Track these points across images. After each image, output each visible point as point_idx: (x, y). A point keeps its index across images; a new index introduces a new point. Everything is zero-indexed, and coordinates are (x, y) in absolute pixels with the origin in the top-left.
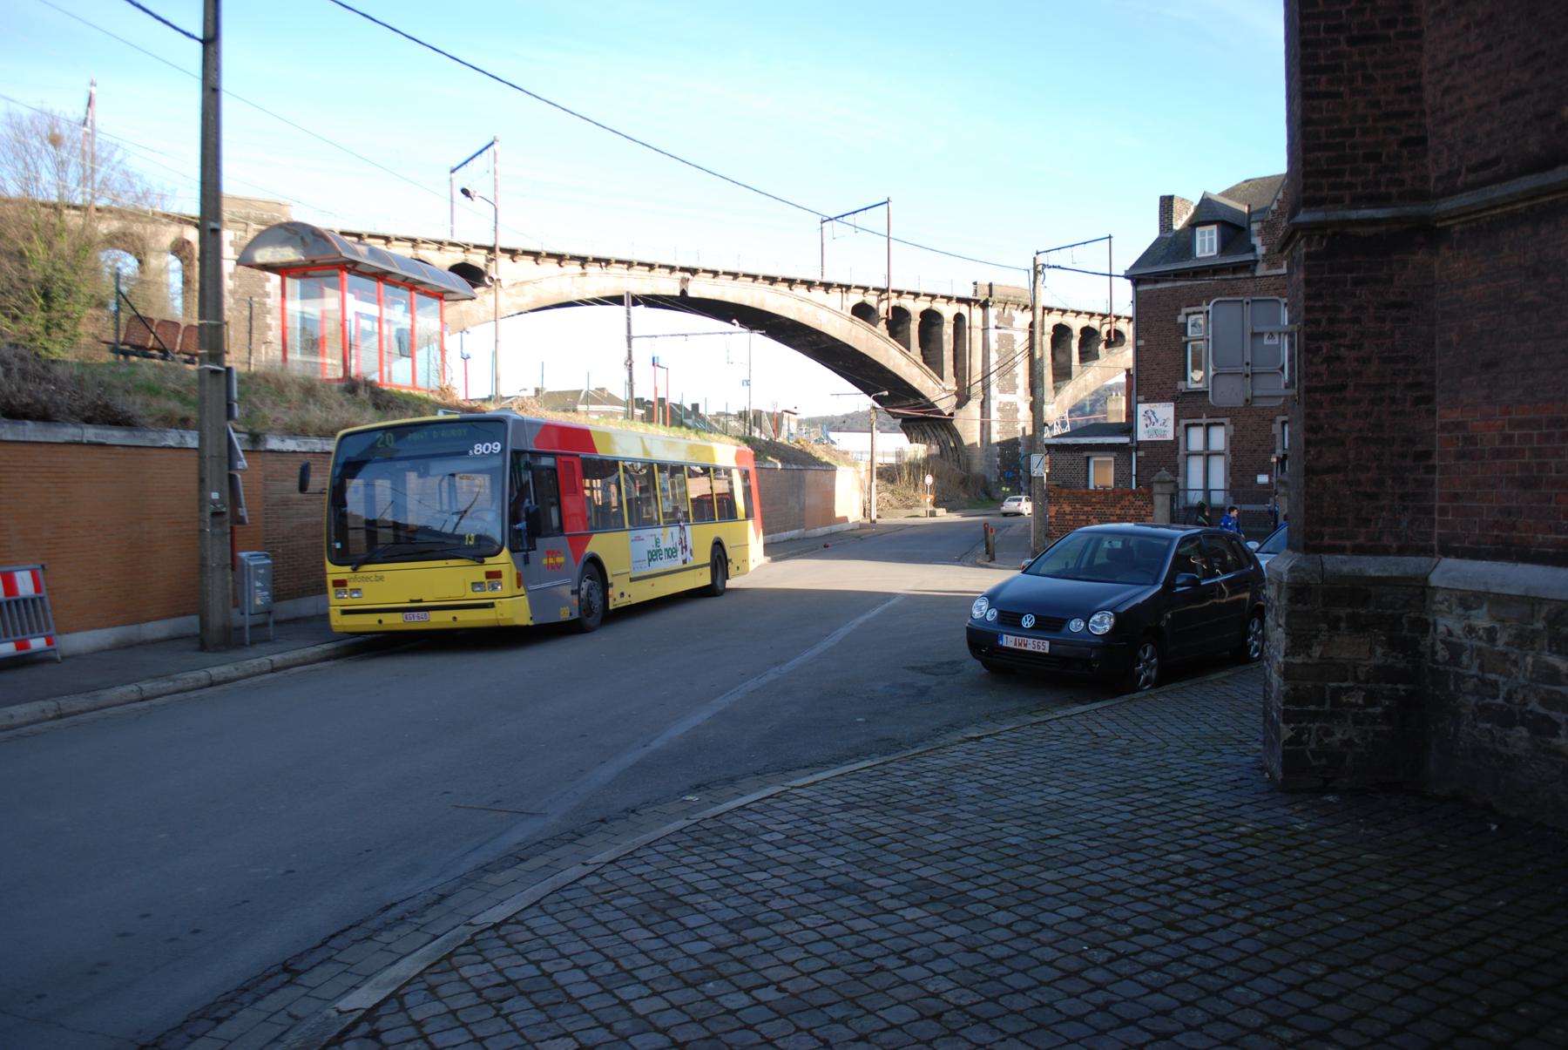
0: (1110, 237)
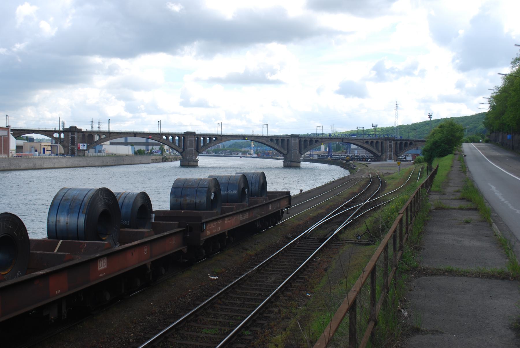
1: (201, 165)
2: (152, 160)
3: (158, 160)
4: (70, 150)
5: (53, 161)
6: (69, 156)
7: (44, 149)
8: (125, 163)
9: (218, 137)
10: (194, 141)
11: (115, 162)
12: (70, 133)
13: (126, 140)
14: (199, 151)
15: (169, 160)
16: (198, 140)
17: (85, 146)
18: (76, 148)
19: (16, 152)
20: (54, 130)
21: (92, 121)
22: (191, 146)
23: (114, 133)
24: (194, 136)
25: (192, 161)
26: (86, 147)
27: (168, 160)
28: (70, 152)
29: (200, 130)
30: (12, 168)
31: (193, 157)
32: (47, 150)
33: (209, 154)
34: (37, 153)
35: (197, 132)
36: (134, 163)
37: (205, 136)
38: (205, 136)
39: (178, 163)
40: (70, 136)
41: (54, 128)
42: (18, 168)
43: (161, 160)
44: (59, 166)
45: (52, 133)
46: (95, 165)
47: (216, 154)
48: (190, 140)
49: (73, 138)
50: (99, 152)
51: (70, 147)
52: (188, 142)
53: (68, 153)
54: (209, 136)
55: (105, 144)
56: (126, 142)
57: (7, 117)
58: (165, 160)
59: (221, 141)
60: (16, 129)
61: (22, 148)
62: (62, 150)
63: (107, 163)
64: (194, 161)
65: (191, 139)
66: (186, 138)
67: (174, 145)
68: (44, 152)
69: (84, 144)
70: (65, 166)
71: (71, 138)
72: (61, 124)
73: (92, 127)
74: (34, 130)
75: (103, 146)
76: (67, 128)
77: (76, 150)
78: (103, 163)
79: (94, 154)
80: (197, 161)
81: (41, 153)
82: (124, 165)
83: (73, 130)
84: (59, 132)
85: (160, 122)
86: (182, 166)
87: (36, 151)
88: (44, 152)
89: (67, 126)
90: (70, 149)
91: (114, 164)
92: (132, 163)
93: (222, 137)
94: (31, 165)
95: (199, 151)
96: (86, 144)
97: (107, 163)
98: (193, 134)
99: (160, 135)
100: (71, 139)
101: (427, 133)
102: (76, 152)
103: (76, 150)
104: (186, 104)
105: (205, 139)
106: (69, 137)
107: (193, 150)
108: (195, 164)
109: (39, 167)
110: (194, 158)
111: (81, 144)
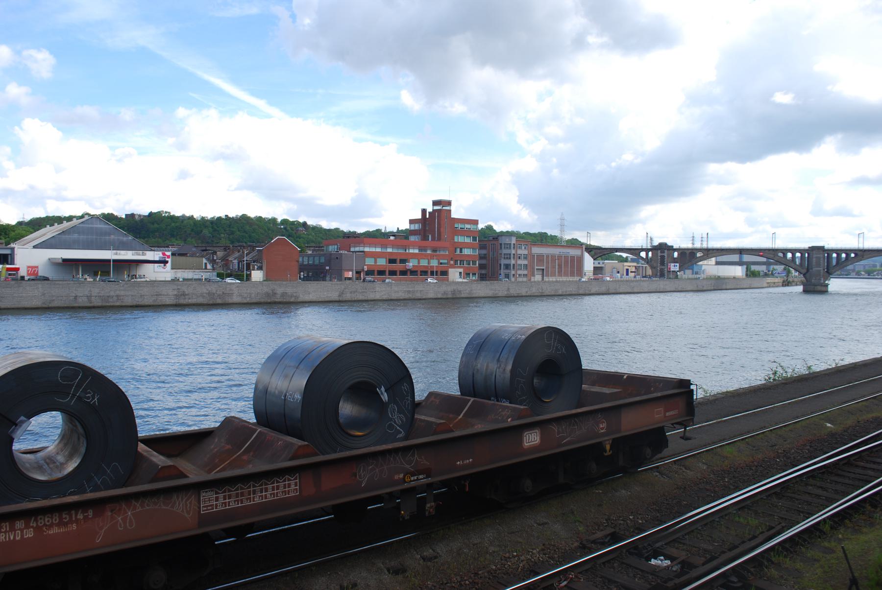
1: (833, 290)
2: (768, 283)
3: (777, 284)
5: (632, 284)
6: (656, 279)
7: (627, 270)
8: (728, 287)
9: (859, 253)
10: (822, 259)
11: (714, 286)
12: (659, 251)
13: (740, 258)
14: (829, 272)
15: (794, 284)
16: (829, 257)
18: (666, 269)
19: (594, 274)
20: (641, 248)
21: (693, 237)
22: (818, 265)
23: (713, 250)
24: (822, 252)
25: (819, 285)
26: (678, 267)
27: (791, 283)
28: (658, 274)
29: (830, 243)
30: (581, 292)
31: (821, 280)
32: (631, 272)
33: (847, 275)
34: (619, 275)
35: (827, 247)
36: (741, 287)
37: (838, 252)
38: (838, 252)
39: (800, 288)
40: (659, 254)
41: (641, 245)
42: (587, 292)
43: (781, 284)
44: (639, 291)
45: (638, 251)
46: (686, 290)
47: (869, 275)
48: (816, 257)
49: (663, 257)
50: (697, 273)
52: (814, 259)
53: (657, 275)
54: (855, 252)
55: (709, 264)
56: (741, 261)
57: (589, 235)
58: (786, 283)
59: (863, 257)
60: (614, 247)
61: (602, 270)
62: (649, 272)
63: (703, 286)
64: (822, 286)
65: (818, 256)
66: (811, 254)
67: (793, 264)
68: (627, 274)
69: (676, 264)
70: (646, 291)
72: (649, 241)
73: (693, 244)
74: (617, 249)
75: (703, 266)
76: (656, 245)
77: (666, 272)
78: (697, 286)
79: (691, 276)
80: (827, 285)
81: (623, 275)
82: (726, 289)
83: (663, 248)
84: (647, 250)
85: (774, 235)
86: (806, 291)
87: (618, 272)
88: (627, 274)
89: (656, 243)
91: (712, 288)
92: (738, 287)
93: (865, 253)
94: (603, 289)
95: (829, 271)
96: (678, 264)
97: (703, 286)
98: (821, 249)
99: (775, 251)
100: (659, 258)
101: (115, 355)
102: (666, 274)
103: (666, 272)
104: (818, 211)
105: (839, 255)
106: (658, 256)
107: (821, 270)
108: (823, 289)
109: (613, 291)
110: (822, 281)
111: (672, 264)
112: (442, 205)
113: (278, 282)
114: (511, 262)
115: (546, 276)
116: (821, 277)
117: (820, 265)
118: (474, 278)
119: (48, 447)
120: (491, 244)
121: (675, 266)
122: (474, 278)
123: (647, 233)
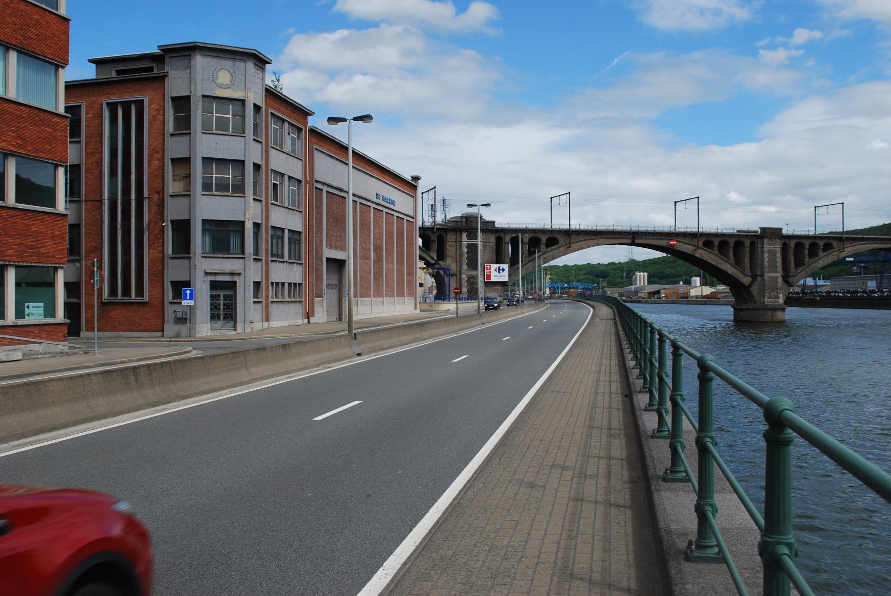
0: (435, 187)
4: (466, 284)
17: (503, 270)
26: (506, 273)
28: (465, 290)
48: (769, 251)
51: (464, 276)
52: (766, 255)
69: (502, 266)
71: (467, 247)
90: (466, 279)
96: (26, 305)
100: (466, 250)
107: (777, 277)
111: (494, 266)
112: (782, 229)
113: (869, 249)
114: (191, 208)
115: (490, 280)
116: (778, 293)
117: (777, 267)
118: (35, 313)
119: (814, 518)
120: (113, 107)
121: (499, 270)
122: (35, 313)
123: (365, 118)
